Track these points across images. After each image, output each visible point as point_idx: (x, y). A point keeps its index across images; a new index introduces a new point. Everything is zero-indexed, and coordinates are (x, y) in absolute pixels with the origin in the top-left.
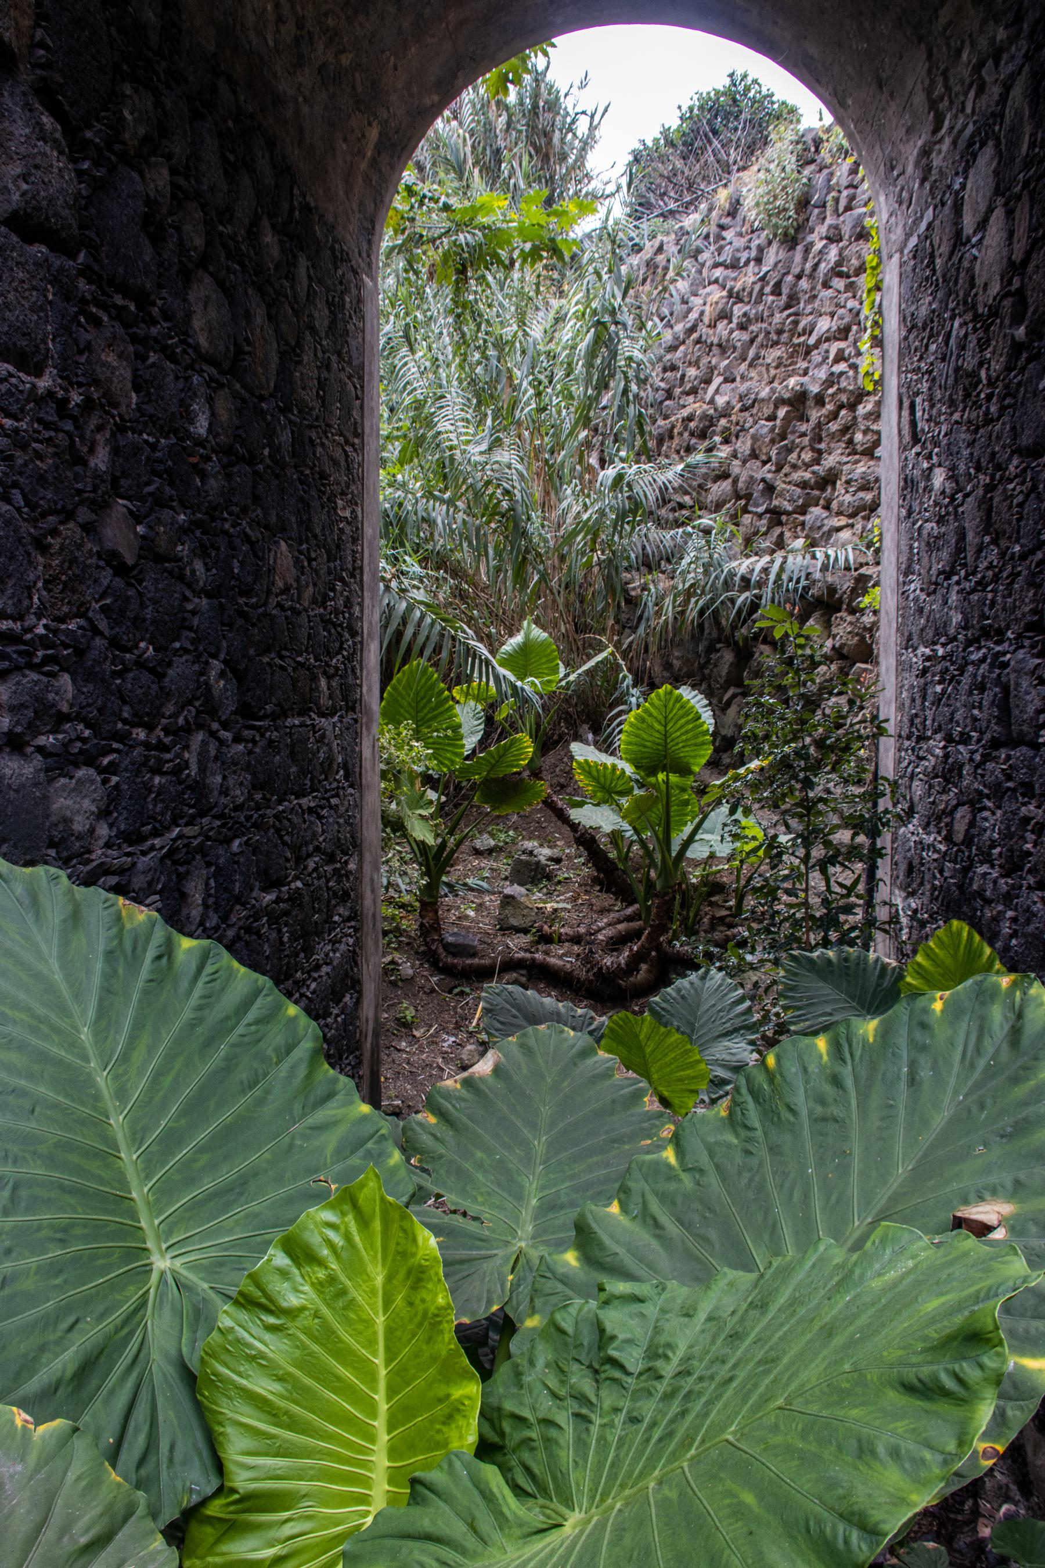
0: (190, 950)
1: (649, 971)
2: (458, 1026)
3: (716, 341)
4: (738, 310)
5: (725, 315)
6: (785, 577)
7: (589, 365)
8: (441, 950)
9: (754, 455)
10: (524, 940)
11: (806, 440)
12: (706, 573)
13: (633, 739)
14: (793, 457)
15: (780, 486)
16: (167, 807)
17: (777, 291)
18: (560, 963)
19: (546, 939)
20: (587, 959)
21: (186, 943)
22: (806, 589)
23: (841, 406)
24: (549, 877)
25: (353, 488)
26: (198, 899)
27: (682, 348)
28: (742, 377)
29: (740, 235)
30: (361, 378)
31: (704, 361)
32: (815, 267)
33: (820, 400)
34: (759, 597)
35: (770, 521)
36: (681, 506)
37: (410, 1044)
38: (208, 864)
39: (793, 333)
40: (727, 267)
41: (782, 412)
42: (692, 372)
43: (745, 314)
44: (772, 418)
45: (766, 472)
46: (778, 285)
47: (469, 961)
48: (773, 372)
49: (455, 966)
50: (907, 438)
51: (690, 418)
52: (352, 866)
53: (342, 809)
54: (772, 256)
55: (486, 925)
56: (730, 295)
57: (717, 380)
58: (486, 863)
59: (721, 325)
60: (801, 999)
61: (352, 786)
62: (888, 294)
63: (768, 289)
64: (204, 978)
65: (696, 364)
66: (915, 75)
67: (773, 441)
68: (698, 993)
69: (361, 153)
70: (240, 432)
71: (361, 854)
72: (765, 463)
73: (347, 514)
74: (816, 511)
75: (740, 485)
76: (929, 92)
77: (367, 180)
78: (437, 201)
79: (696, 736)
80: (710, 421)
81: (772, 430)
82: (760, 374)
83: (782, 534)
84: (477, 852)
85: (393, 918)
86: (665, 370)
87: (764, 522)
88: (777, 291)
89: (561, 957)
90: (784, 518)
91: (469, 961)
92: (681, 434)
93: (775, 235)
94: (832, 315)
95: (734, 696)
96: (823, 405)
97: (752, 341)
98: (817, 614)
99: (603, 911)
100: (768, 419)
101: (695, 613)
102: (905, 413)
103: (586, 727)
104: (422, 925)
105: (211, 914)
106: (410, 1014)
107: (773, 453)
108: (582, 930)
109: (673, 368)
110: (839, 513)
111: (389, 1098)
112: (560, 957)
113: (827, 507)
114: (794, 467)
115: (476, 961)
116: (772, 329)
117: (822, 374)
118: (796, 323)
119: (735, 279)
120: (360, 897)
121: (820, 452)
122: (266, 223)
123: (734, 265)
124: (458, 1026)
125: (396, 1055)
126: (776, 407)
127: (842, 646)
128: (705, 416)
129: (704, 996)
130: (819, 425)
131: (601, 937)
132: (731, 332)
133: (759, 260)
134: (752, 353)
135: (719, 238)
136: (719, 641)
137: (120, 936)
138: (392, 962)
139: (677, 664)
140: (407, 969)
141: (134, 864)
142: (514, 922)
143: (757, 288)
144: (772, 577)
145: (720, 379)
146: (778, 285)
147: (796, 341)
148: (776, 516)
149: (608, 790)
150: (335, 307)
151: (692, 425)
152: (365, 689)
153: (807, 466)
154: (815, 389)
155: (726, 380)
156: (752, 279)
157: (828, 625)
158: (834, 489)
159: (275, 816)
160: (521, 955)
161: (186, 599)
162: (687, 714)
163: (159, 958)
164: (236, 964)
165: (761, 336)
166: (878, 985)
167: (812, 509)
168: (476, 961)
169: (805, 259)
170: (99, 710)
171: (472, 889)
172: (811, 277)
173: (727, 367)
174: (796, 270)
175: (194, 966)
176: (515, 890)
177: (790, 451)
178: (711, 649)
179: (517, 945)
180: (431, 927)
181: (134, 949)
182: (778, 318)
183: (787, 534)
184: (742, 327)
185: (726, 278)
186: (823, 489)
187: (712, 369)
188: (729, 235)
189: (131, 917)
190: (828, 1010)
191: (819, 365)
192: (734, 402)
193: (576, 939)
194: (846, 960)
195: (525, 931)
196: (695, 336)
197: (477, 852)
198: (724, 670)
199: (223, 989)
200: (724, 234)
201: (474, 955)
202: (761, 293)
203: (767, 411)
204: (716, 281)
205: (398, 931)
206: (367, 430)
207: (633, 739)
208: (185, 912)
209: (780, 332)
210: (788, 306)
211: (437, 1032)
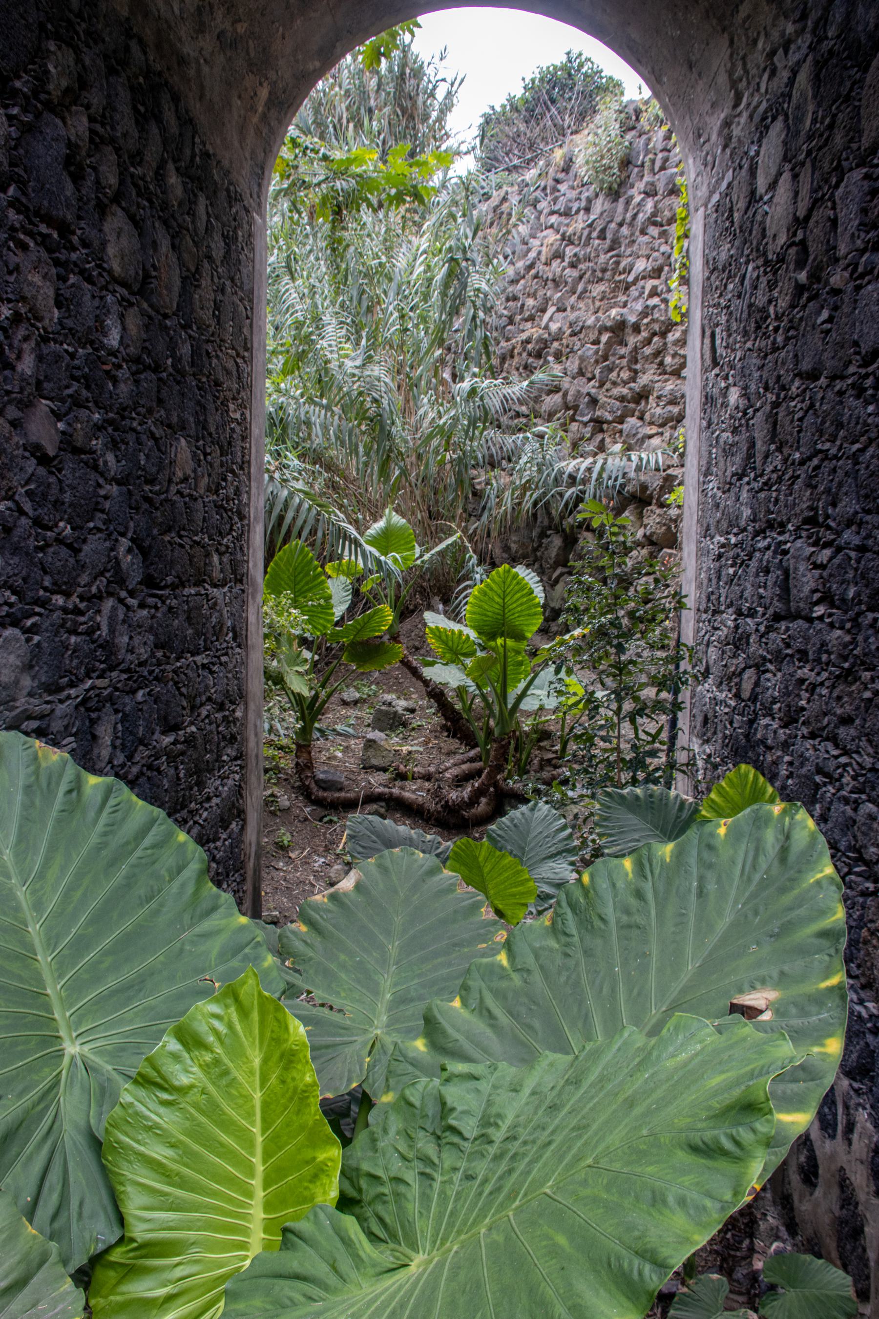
0: (96, 786)
1: (488, 804)
2: (327, 849)
3: (551, 276)
4: (570, 251)
5: (558, 255)
6: (605, 476)
7: (444, 294)
8: (313, 785)
9: (581, 373)
10: (384, 777)
11: (624, 362)
12: (540, 471)
13: (477, 610)
14: (613, 376)
15: (602, 399)
16: (81, 663)
17: (602, 236)
18: (413, 796)
19: (402, 776)
20: (436, 794)
21: (93, 780)
22: (623, 486)
23: (654, 334)
24: (404, 725)
25: (243, 394)
26: (108, 740)
27: (522, 282)
28: (572, 308)
29: (573, 188)
30: (251, 301)
31: (540, 293)
32: (635, 216)
33: (636, 329)
34: (583, 492)
35: (594, 428)
36: (518, 415)
37: (287, 864)
38: (116, 711)
39: (615, 271)
40: (561, 215)
41: (604, 338)
42: (530, 302)
43: (575, 255)
44: (596, 342)
45: (590, 387)
46: (603, 231)
47: (337, 795)
48: (598, 304)
49: (325, 799)
50: (708, 362)
51: (528, 341)
52: (239, 714)
53: (231, 666)
54: (599, 206)
55: (352, 764)
56: (563, 238)
57: (551, 310)
58: (352, 712)
59: (555, 263)
60: (613, 828)
61: (239, 646)
62: (694, 241)
63: (595, 234)
64: (107, 810)
65: (534, 295)
66: (719, 58)
67: (597, 362)
68: (528, 822)
69: (253, 109)
70: (147, 344)
71: (246, 704)
72: (590, 380)
73: (238, 416)
74: (632, 421)
75: (569, 398)
76: (731, 73)
77: (258, 132)
78: (317, 152)
79: (529, 608)
80: (545, 344)
81: (597, 352)
82: (587, 305)
83: (603, 440)
84: (345, 703)
85: (273, 758)
86: (508, 300)
87: (589, 429)
88: (602, 236)
89: (414, 792)
90: (605, 426)
91: (337, 795)
92: (520, 354)
93: (601, 189)
94: (648, 257)
95: (562, 575)
96: (639, 332)
97: (581, 277)
98: (631, 507)
99: (450, 754)
100: (593, 343)
101: (530, 505)
102: (707, 341)
103: (437, 598)
104: (297, 764)
105: (118, 753)
106: (286, 839)
107: (597, 372)
108: (432, 769)
109: (515, 298)
110: (651, 423)
111: (269, 909)
112: (414, 792)
113: (641, 418)
114: (614, 384)
115: (343, 794)
116: (598, 268)
117: (639, 306)
118: (617, 263)
119: (567, 225)
120: (245, 740)
121: (636, 372)
122: (171, 166)
123: (567, 213)
124: (327, 849)
125: (274, 873)
126: (600, 333)
127: (652, 534)
128: (540, 340)
129: (533, 824)
130: (635, 349)
131: (447, 775)
132: (564, 269)
133: (587, 210)
134: (580, 288)
135: (555, 190)
136: (550, 528)
137: (37, 773)
138: (272, 795)
139: (514, 547)
140: (284, 801)
141: (53, 711)
142: (375, 762)
143: (586, 233)
144: (595, 476)
145: (554, 309)
146: (603, 231)
147: (617, 278)
148: (599, 424)
149: (455, 652)
150: (229, 240)
151: (530, 346)
152: (251, 564)
153: (625, 383)
154: (632, 319)
155: (559, 310)
156: (581, 226)
157: (640, 516)
158: (647, 403)
159: (174, 671)
160: (381, 789)
161: (99, 486)
162: (522, 589)
163: (70, 792)
164: (134, 798)
165: (589, 273)
166: (678, 817)
167: (629, 419)
168: (343, 794)
169: (626, 210)
170: (24, 579)
171: (340, 734)
172: (631, 225)
173: (560, 299)
174: (618, 219)
175: (99, 799)
176: (376, 735)
177: (610, 370)
178: (543, 535)
179: (377, 782)
180: (304, 767)
181: (49, 784)
182: (603, 258)
183: (608, 440)
184: (573, 265)
185: (560, 224)
186: (638, 403)
187: (547, 300)
188: (563, 187)
189: (46, 757)
190: (636, 837)
191: (636, 299)
192: (565, 328)
193: (428, 777)
194: (651, 796)
195: (385, 770)
196: (533, 272)
197: (345, 703)
198: (553, 552)
199: (124, 819)
200: (559, 186)
201: (341, 789)
202: (589, 238)
203: (593, 336)
204: (552, 226)
205: (277, 769)
206: (255, 345)
207: (477, 610)
208: (96, 751)
209: (604, 271)
210: (611, 249)
211: (309, 854)
